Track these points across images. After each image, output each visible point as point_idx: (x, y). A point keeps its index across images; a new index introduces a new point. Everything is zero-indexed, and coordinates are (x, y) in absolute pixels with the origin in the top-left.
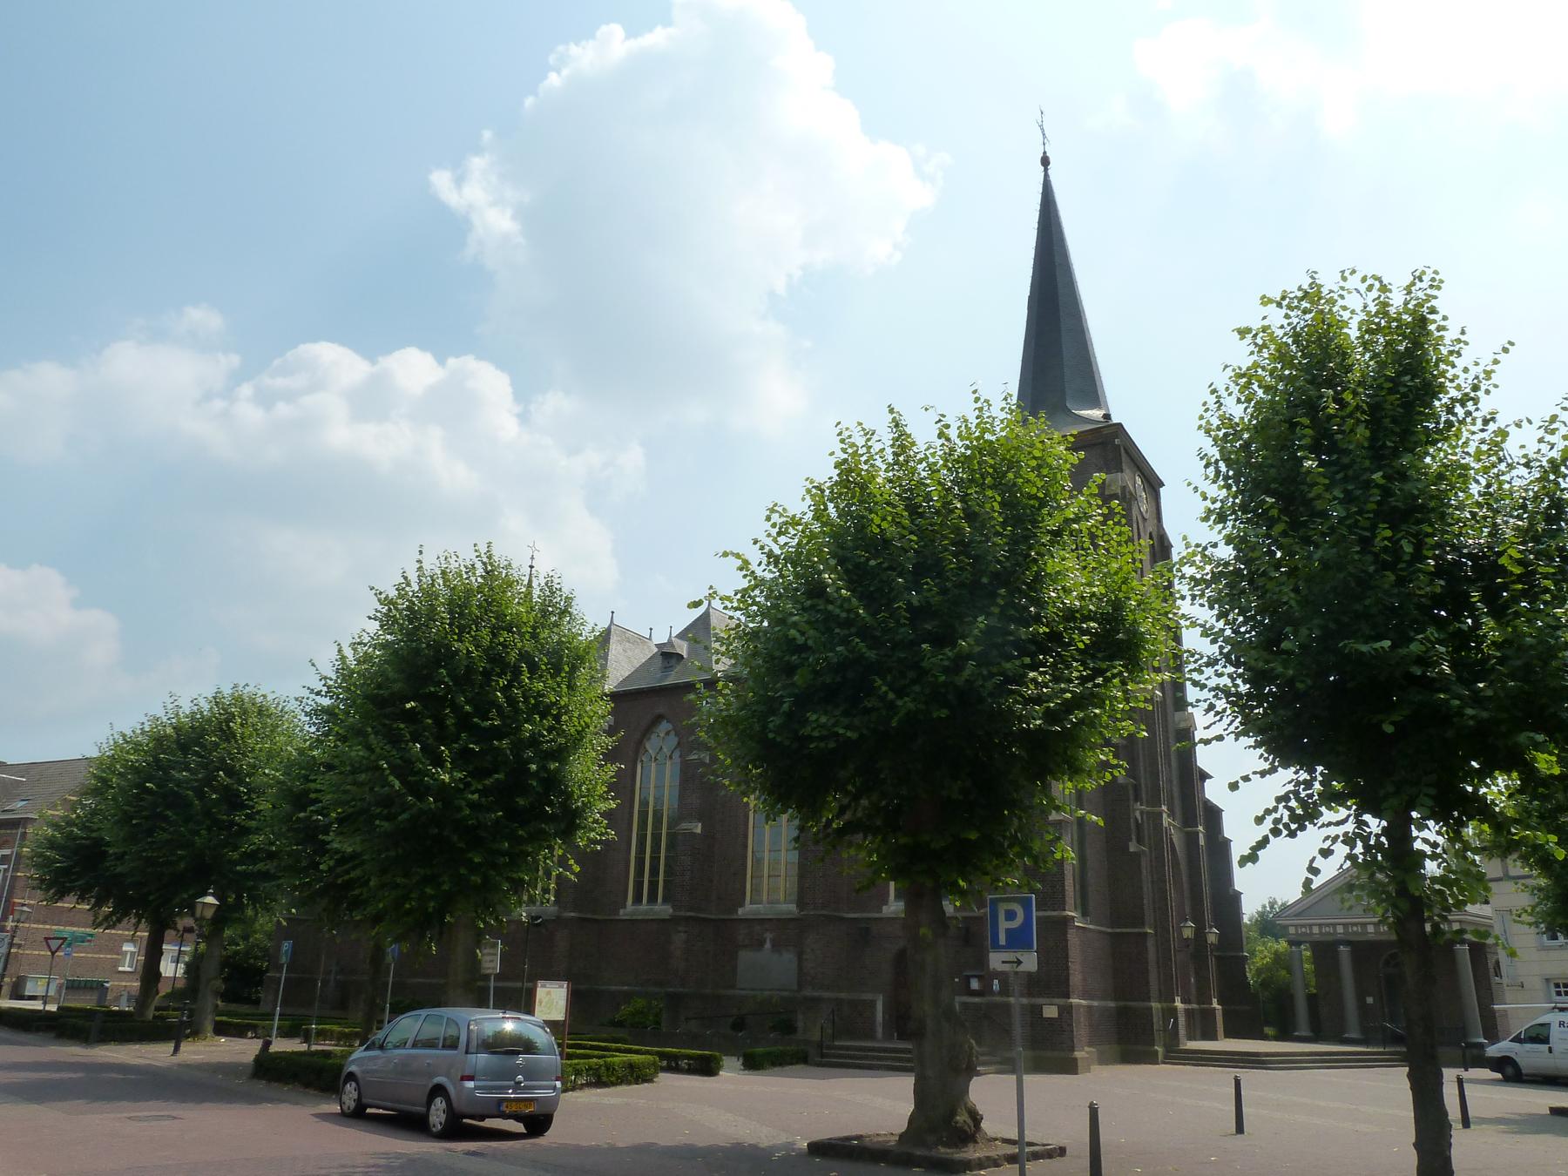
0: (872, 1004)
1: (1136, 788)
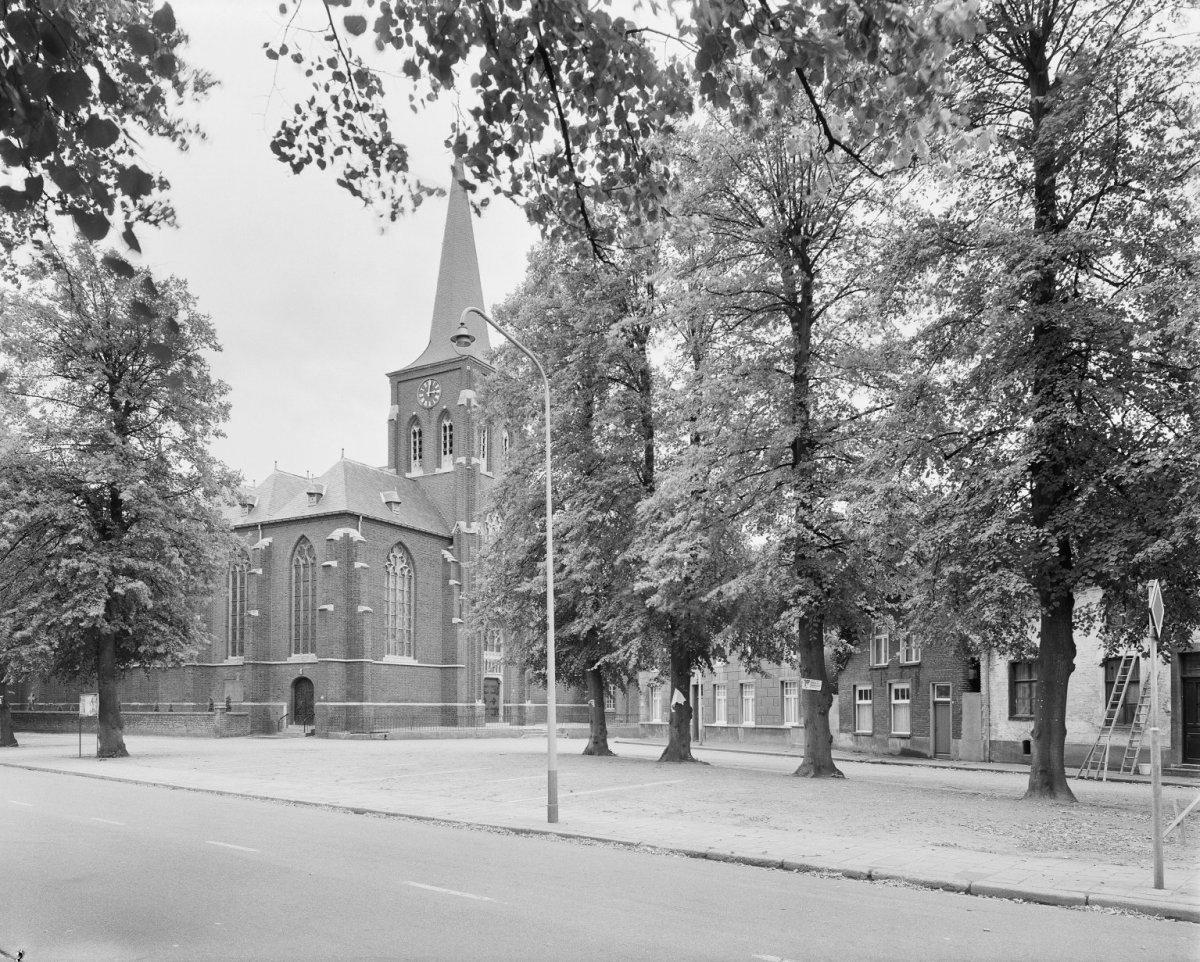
0: (282, 707)
1: (460, 587)
